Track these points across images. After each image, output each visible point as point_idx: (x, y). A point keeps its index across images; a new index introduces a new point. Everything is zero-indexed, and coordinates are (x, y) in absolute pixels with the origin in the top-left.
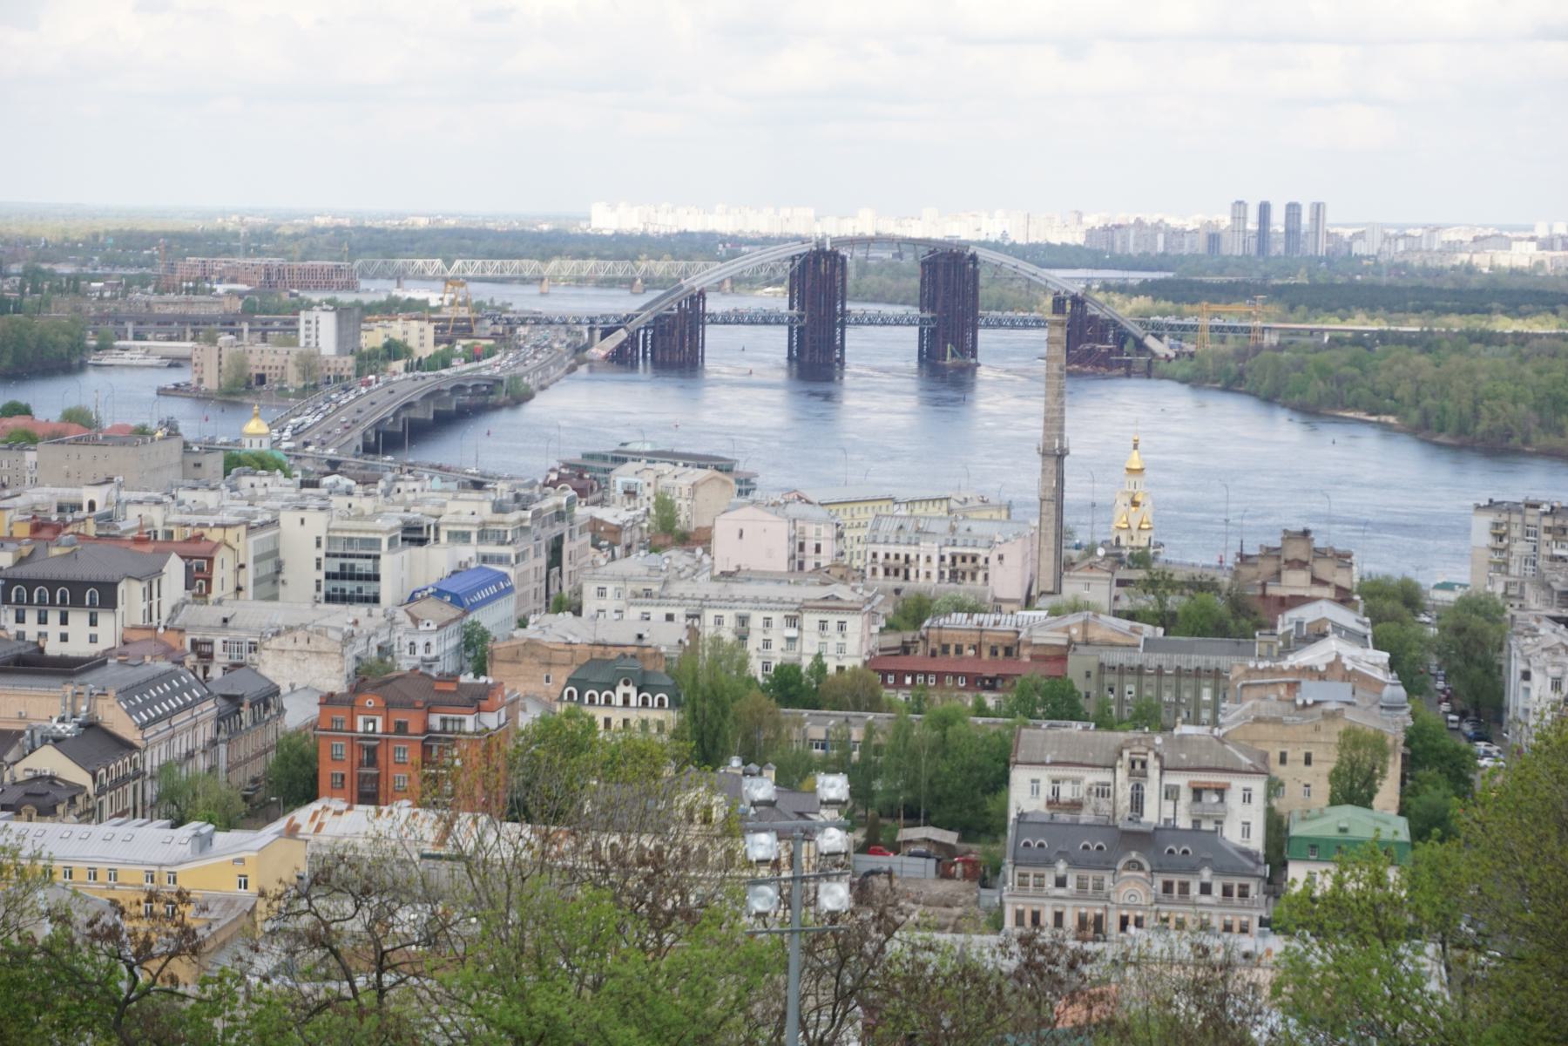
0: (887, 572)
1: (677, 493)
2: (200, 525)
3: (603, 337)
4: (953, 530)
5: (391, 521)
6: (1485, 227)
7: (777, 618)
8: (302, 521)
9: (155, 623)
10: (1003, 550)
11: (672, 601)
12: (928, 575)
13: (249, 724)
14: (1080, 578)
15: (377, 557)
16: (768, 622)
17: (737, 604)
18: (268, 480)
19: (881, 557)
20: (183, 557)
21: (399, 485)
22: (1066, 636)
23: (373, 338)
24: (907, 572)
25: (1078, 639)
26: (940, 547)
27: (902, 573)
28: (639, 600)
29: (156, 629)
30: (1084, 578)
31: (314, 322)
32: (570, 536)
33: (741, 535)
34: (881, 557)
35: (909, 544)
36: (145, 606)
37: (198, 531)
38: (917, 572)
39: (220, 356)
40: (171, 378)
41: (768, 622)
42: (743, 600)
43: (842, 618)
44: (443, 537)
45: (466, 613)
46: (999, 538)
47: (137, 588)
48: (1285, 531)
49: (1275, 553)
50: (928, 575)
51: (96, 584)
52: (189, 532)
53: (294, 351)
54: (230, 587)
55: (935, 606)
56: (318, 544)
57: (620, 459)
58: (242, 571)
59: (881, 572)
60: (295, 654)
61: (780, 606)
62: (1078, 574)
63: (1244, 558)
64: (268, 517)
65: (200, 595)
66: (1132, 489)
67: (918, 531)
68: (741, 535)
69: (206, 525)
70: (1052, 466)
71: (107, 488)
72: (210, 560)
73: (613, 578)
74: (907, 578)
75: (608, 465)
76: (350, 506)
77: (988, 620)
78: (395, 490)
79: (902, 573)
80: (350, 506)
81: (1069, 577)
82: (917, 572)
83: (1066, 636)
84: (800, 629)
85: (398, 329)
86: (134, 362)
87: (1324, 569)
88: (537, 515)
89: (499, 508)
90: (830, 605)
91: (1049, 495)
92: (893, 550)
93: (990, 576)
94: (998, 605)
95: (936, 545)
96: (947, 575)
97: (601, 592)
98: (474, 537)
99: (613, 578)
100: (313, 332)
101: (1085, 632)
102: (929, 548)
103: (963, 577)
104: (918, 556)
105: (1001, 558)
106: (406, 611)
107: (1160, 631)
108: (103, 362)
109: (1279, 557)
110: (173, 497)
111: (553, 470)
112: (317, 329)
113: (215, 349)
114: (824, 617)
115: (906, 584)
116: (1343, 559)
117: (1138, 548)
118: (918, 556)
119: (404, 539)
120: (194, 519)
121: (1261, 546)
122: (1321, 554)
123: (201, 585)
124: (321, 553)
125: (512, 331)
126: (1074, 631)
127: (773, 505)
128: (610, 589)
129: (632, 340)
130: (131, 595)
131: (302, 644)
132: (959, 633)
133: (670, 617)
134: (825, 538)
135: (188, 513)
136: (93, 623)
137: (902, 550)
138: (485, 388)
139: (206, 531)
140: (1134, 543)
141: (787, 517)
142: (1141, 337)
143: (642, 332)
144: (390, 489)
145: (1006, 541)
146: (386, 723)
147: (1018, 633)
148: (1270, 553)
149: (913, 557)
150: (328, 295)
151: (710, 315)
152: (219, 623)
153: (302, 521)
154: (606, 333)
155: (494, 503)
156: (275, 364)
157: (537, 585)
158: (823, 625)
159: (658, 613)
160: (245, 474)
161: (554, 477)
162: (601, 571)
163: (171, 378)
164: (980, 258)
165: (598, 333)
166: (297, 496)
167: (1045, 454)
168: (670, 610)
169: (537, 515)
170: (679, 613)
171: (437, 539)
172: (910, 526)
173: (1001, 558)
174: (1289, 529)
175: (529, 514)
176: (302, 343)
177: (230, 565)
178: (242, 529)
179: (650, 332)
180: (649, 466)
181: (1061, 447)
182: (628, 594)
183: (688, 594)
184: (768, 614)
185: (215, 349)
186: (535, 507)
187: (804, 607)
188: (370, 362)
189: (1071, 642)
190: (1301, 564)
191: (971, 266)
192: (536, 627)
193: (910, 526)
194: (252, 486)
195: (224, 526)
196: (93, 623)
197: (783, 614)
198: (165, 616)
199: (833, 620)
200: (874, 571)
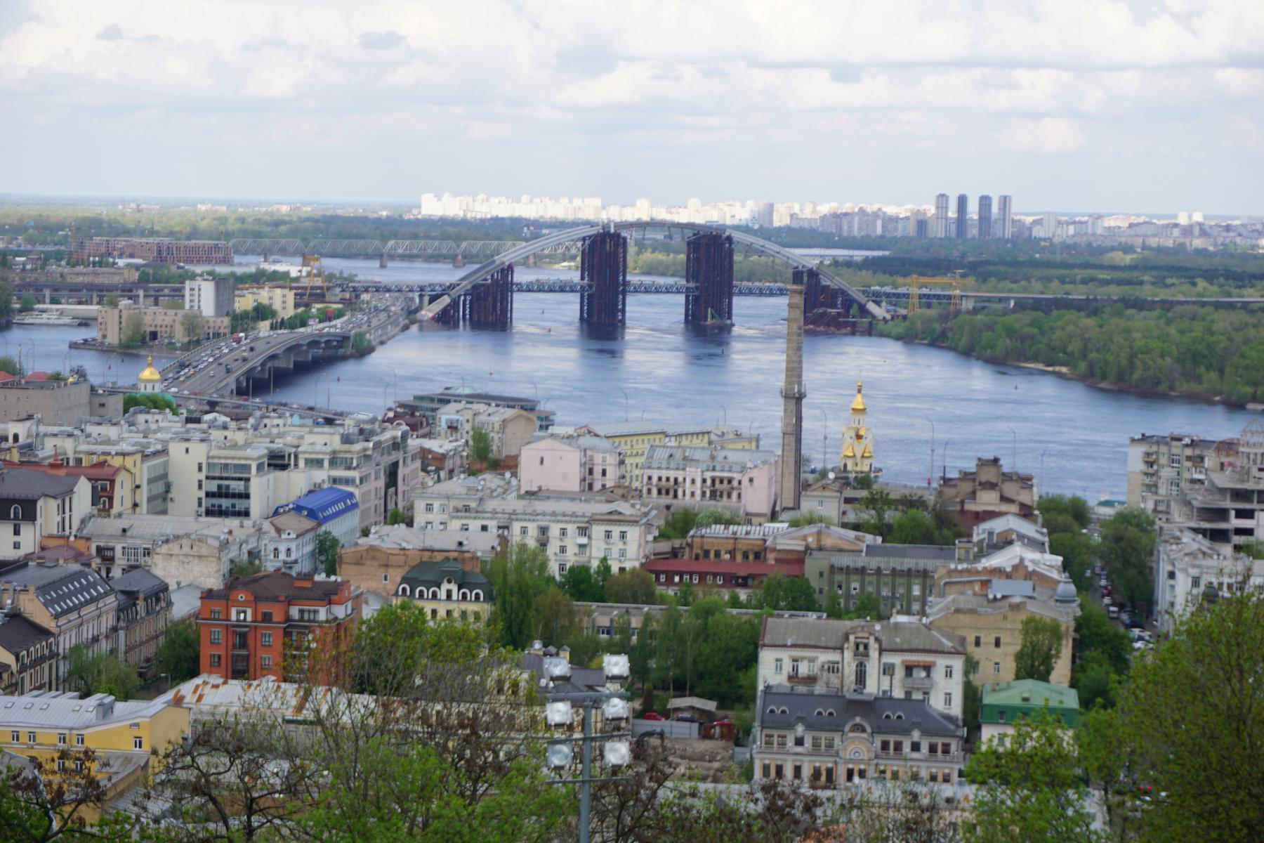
0: (659, 492)
1: (490, 428)
2: (104, 453)
3: (431, 302)
4: (713, 458)
5: (259, 450)
6: (1139, 216)
7: (571, 529)
8: (187, 451)
9: (67, 533)
10: (754, 473)
11: (486, 515)
12: (693, 494)
13: (143, 615)
14: (815, 496)
15: (248, 480)
16: (563, 532)
17: (538, 517)
18: (159, 417)
19: (655, 479)
20: (90, 480)
21: (266, 421)
22: (804, 543)
23: (245, 302)
24: (676, 492)
25: (813, 546)
26: (703, 472)
27: (672, 493)
28: (459, 514)
29: (68, 537)
30: (818, 496)
31: (197, 289)
32: (404, 462)
33: (542, 462)
34: (655, 479)
35: (677, 469)
36: (59, 519)
37: (102, 458)
38: (684, 492)
39: (120, 317)
40: (80, 335)
41: (563, 532)
42: (544, 514)
43: (623, 529)
44: (301, 463)
45: (320, 525)
46: (750, 465)
47: (53, 504)
48: (979, 459)
49: (971, 477)
50: (693, 494)
51: (19, 501)
52: (95, 459)
53: (181, 313)
54: (128, 503)
55: (699, 519)
56: (200, 469)
57: (444, 401)
58: (138, 491)
59: (655, 491)
60: (181, 558)
61: (573, 519)
62: (814, 493)
63: (946, 481)
64: (159, 447)
65: (104, 510)
66: (856, 425)
67: (685, 458)
68: (542, 462)
69: (109, 454)
70: (792, 407)
71: (28, 424)
72: (112, 482)
73: (439, 496)
74: (675, 496)
75: (435, 405)
76: (226, 438)
77: (741, 530)
78: (262, 425)
79: (672, 493)
80: (226, 438)
81: (806, 496)
82: (684, 492)
83: (804, 543)
84: (590, 538)
85: (264, 295)
86: (51, 322)
87: (1010, 489)
88: (377, 445)
89: (346, 440)
90: (614, 518)
91: (789, 429)
92: (664, 474)
93: (743, 495)
94: (749, 519)
95: (699, 470)
96: (708, 494)
97: (429, 508)
98: (326, 464)
99: (439, 496)
100: (196, 298)
101: (819, 540)
102: (694, 472)
103: (721, 496)
104: (685, 479)
105: (751, 480)
106: (271, 523)
107: (879, 539)
108: (25, 321)
109: (974, 480)
110: (82, 431)
111: (390, 409)
112: (199, 295)
113: (116, 312)
114: (609, 528)
115: (675, 502)
116: (1025, 481)
117: (862, 472)
118: (685, 479)
119: (269, 465)
120: (100, 449)
121: (960, 471)
122: (1007, 477)
123: (104, 502)
124: (202, 476)
125: (357, 297)
126: (810, 539)
127: (568, 438)
128: (436, 505)
129: (455, 303)
130: (48, 510)
131: (186, 550)
132: (718, 541)
133: (484, 528)
134: (610, 465)
135: (94, 444)
136: (17, 532)
137: (672, 474)
138: (335, 343)
139: (109, 458)
140: (858, 469)
141: (579, 447)
142: (863, 302)
143: (462, 298)
144: (259, 424)
145: (755, 467)
146: (255, 614)
147: (765, 541)
148: (966, 476)
149: (680, 479)
150: (208, 268)
151: (517, 284)
152: (119, 533)
153: (187, 451)
154: (433, 299)
155: (342, 435)
156: (166, 323)
157: (377, 502)
158: (608, 534)
159: (475, 525)
160: (141, 412)
161: (391, 414)
162: (430, 490)
163: (80, 335)
164: (734, 239)
165: (426, 299)
166: (183, 430)
167: (787, 397)
168: (485, 522)
169: (377, 445)
170: (492, 524)
171: (296, 465)
172: (678, 455)
173: (751, 480)
174: (984, 458)
175: (371, 445)
176: (187, 306)
177: (128, 486)
178: (138, 457)
179: (469, 298)
180: (468, 406)
181: (799, 391)
182: (451, 510)
183: (500, 509)
184: (563, 526)
185: (116, 312)
186: (376, 439)
187: (594, 520)
188: (243, 321)
189: (807, 548)
190: (992, 486)
191: (727, 245)
192: (377, 536)
193: (678, 455)
194: (147, 422)
195: (124, 454)
196: (17, 532)
197: (576, 525)
198: (75, 526)
199: (616, 530)
200: (649, 491)
